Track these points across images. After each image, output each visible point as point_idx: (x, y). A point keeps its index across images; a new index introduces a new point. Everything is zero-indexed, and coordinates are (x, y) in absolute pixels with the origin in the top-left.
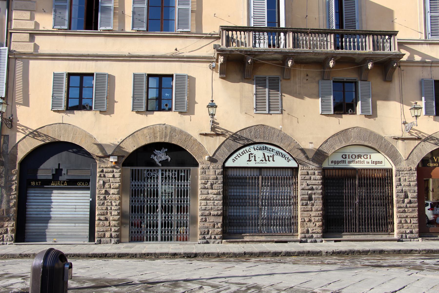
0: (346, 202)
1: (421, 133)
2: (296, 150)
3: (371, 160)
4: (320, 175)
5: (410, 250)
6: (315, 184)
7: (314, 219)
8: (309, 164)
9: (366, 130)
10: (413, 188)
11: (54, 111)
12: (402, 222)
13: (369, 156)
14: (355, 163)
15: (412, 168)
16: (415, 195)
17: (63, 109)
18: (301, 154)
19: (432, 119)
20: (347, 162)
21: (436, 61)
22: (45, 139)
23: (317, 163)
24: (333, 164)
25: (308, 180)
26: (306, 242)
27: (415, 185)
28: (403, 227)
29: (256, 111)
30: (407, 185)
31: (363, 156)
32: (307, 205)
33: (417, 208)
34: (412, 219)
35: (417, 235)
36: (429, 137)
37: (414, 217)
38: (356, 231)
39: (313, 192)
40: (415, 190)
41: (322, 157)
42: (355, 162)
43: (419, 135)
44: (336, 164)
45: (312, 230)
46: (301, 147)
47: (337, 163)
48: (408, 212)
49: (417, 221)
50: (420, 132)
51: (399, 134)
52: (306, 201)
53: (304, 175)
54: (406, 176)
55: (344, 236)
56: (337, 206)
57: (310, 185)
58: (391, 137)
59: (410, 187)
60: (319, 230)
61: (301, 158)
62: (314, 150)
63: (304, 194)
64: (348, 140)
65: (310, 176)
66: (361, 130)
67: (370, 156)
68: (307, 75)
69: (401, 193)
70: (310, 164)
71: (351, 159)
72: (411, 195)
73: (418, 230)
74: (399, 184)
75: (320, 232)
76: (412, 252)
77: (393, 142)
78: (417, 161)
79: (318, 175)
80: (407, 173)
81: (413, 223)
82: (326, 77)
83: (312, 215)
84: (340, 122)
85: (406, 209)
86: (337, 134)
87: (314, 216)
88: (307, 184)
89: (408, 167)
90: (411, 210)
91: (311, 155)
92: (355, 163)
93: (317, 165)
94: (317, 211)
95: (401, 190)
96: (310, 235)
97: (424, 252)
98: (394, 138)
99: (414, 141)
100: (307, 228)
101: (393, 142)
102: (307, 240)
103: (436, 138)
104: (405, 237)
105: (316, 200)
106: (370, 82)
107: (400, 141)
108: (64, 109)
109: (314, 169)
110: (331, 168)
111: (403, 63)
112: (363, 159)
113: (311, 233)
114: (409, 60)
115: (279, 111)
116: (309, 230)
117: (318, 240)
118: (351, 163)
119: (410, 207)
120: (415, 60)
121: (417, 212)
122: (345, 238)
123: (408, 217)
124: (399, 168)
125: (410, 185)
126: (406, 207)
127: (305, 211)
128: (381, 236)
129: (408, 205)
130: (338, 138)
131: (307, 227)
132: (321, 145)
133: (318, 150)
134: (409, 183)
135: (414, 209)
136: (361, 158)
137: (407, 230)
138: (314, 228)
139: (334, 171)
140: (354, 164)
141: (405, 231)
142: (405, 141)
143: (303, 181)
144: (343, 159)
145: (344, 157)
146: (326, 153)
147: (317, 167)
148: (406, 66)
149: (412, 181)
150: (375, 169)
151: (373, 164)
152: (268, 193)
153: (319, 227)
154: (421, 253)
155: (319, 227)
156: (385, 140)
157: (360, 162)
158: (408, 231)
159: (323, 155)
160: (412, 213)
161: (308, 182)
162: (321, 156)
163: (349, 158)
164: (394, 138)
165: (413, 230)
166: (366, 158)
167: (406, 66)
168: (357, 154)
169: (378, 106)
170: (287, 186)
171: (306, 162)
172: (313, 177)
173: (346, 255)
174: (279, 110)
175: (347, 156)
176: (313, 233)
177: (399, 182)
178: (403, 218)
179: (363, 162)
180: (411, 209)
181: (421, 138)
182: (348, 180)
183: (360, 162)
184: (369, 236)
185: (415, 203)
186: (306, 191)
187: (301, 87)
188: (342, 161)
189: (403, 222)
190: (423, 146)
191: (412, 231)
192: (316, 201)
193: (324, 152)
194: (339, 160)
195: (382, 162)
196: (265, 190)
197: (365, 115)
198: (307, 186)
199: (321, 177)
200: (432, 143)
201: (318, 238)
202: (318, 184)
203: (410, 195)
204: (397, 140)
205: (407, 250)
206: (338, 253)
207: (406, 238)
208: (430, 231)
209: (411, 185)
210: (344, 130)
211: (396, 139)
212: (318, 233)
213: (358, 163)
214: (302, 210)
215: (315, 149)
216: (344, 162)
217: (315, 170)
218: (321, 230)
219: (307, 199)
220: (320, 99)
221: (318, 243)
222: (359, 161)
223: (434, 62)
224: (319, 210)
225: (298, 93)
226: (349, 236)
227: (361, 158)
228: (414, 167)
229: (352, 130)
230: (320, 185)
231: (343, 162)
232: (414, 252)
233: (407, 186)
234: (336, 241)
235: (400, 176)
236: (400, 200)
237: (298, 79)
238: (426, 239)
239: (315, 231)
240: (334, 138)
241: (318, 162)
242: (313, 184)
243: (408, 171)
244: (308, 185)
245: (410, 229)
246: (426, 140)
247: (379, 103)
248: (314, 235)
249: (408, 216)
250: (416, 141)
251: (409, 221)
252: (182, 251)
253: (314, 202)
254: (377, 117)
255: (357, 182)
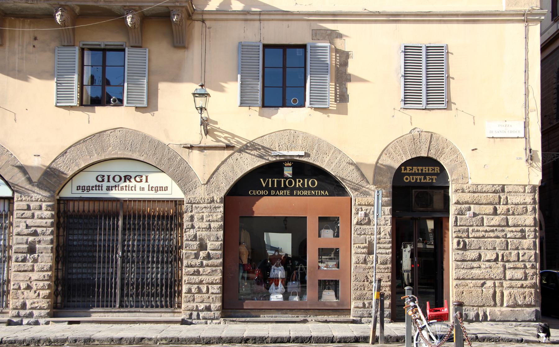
0: (100, 257)
1: (236, 138)
2: (10, 167)
3: (147, 184)
4: (49, 210)
5: (140, 338)
6: (40, 225)
7: (36, 285)
8: (31, 191)
9: (135, 133)
10: (216, 233)
11: (316, 109)
12: (191, 291)
13: (144, 178)
14: (120, 189)
15: (215, 198)
16: (217, 245)
17: (76, 105)
18: (18, 175)
19: (258, 113)
20: (104, 188)
21: (267, 11)
22: (264, 153)
23: (46, 190)
24: (80, 191)
25: (29, 218)
26: (20, 323)
27: (219, 228)
28: (194, 300)
29: (405, 104)
30: (205, 228)
31: (133, 177)
32: (24, 260)
33: (221, 268)
34: (210, 286)
35: (218, 314)
36: (249, 145)
37: (214, 282)
38: (115, 306)
39: (37, 239)
40: (219, 236)
41: (55, 179)
42: (120, 188)
43: (231, 141)
44: (85, 192)
45: (32, 304)
46: (19, 163)
47: (87, 190)
48: (204, 273)
49: (218, 289)
50: (234, 136)
51: (195, 140)
52: (23, 255)
53: (22, 210)
54: (203, 212)
55: (93, 315)
56: (85, 262)
57: (32, 226)
58: (181, 145)
59: (210, 231)
60: (44, 303)
61: (18, 182)
62: (41, 168)
63: (21, 242)
64: (103, 150)
65: (33, 211)
66: (127, 133)
67: (147, 177)
68: (35, 39)
69: (193, 241)
70: (34, 192)
71: (112, 183)
72: (211, 245)
73: (220, 304)
74: (190, 226)
75: (45, 308)
76: (143, 342)
77: (184, 154)
78: (225, 187)
79: (46, 210)
80: (205, 207)
81: (212, 293)
82: (66, 41)
83: (33, 278)
84: (90, 120)
85: (201, 270)
86: (84, 140)
87: (36, 280)
88: (27, 225)
89: (207, 197)
90: (209, 271)
91: (35, 177)
92: (120, 189)
93: (47, 194)
94: (41, 271)
95: (193, 236)
96: (28, 312)
97: (164, 342)
98: (183, 147)
99: (220, 151)
100: (22, 300)
101: (184, 154)
102: (22, 321)
103: (262, 146)
104: (196, 317)
105: (42, 253)
106: (147, 50)
107: (196, 152)
108: (77, 104)
109: (39, 200)
110: (76, 198)
111: (209, 14)
112: (133, 183)
113: (29, 309)
114: (220, 9)
115: (443, 104)
116: (27, 303)
117: (42, 321)
118: (112, 190)
119: (208, 266)
120: (231, 8)
121: (221, 274)
122: (95, 317)
123: (204, 282)
124: (191, 199)
125: (210, 228)
126: (202, 265)
127: (20, 271)
128: (159, 314)
129: (205, 262)
130: (86, 147)
131: (23, 298)
132: (55, 159)
133: (49, 167)
134: (208, 223)
135: (214, 269)
136: (130, 181)
137: (201, 304)
138: (35, 300)
139: (81, 203)
140: (117, 192)
141: (197, 306)
142: (205, 151)
143: (21, 220)
144: (98, 183)
145: (100, 179)
146: (63, 173)
147: (46, 196)
148: (215, 20)
149: (214, 221)
150: (154, 201)
151: (151, 192)
152: (167, 242)
153: (44, 298)
154: (158, 344)
155: (44, 298)
156: (169, 149)
157: (127, 188)
158: (202, 306)
159: (58, 176)
160: (211, 275)
161: (30, 222)
162: (54, 177)
163: (109, 181)
164: (183, 147)
165: (212, 305)
166: (139, 180)
167: (215, 20)
168: (122, 175)
169: (160, 92)
170: (158, 230)
171: (26, 189)
172: (37, 213)
173: (24, 346)
174: (444, 102)
175: (106, 178)
176: (32, 308)
177: (190, 223)
178: (195, 284)
179: (133, 188)
180: (209, 269)
181: (233, 147)
182: (105, 218)
183: (127, 188)
184: (138, 314)
185: (218, 258)
186: (24, 237)
187: (22, 59)
188: (96, 186)
189: (193, 291)
190: (237, 160)
191: (210, 306)
192: (42, 254)
193: (59, 171)
194: (91, 185)
195: (144, 188)
196: (163, 236)
197: (136, 107)
198: (26, 228)
199: (51, 214)
200: (254, 155)
201: (41, 317)
202: (46, 225)
203: (210, 245)
204: (190, 151)
205: (134, 339)
206: (11, 343)
207: (198, 318)
208: (245, 307)
209: (212, 227)
210: (96, 134)
211: (188, 148)
212: (41, 309)
213: (124, 189)
214: (16, 269)
215: (44, 166)
216: (100, 188)
217: (41, 201)
218: (48, 303)
219: (26, 250)
220: (55, 79)
221: (41, 326)
222: (126, 186)
223: (263, 12)
224: (45, 269)
225: (17, 69)
226: (102, 314)
227: (130, 181)
228: (219, 195)
229: (111, 132)
230: (49, 227)
231: (97, 188)
232: (146, 342)
233: (204, 229)
234: (70, 323)
235: (193, 212)
236: (191, 253)
237: (19, 45)
238: (231, 321)
239: (36, 305)
240: (78, 146)
241: (47, 187)
242: (36, 225)
243: (207, 203)
244: (27, 227)
245: (206, 303)
246: (244, 149)
247: (162, 86)
248: (36, 313)
249: (203, 281)
250: (226, 151)
251: (204, 290)
252: (293, 335)
253: (38, 256)
254: (157, 110)
255: (120, 223)
